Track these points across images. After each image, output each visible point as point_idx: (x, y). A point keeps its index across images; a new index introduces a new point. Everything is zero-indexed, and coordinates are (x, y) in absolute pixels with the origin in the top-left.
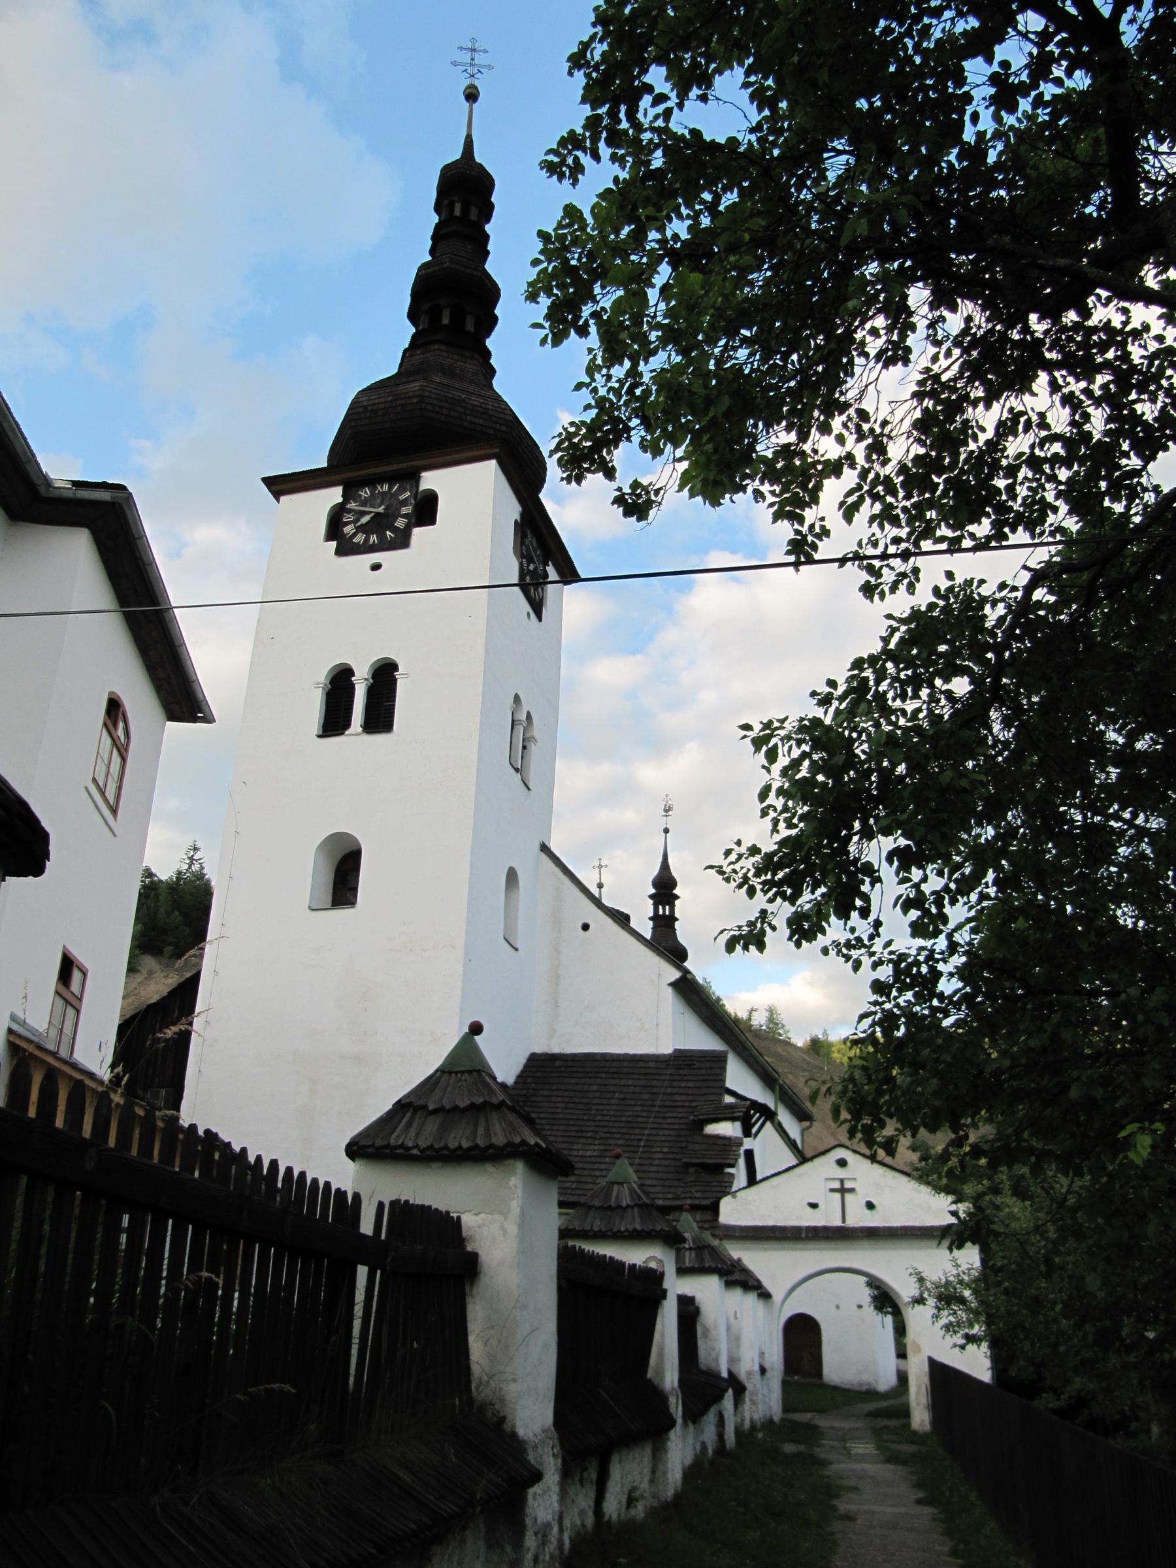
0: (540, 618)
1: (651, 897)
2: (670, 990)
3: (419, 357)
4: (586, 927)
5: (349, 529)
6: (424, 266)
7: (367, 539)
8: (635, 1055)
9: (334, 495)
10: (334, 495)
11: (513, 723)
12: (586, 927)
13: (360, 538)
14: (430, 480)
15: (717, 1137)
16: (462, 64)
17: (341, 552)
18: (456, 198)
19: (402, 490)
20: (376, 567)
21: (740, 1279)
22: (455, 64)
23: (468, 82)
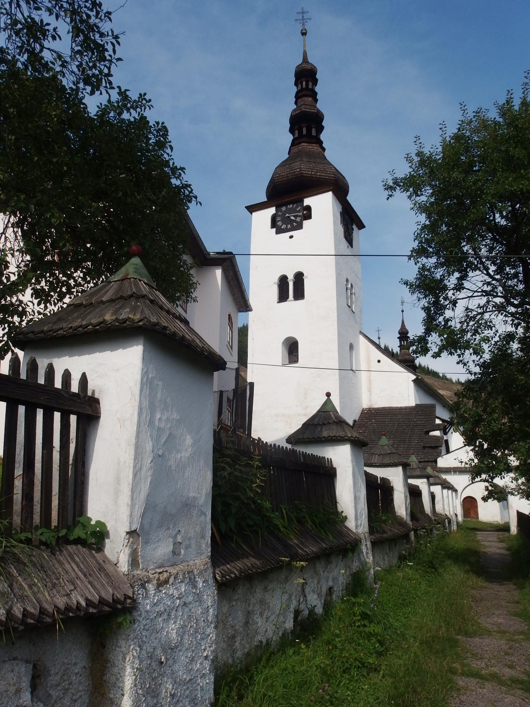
0: (352, 247)
1: (398, 338)
2: (412, 382)
3: (295, 149)
4: (379, 361)
5: (279, 223)
6: (294, 110)
7: (287, 226)
8: (401, 407)
9: (272, 210)
10: (272, 210)
11: (347, 289)
12: (379, 361)
13: (284, 227)
14: (307, 202)
15: (434, 436)
16: (299, 20)
17: (277, 233)
18: (303, 80)
19: (297, 207)
20: (291, 237)
21: (447, 486)
22: (296, 20)
23: (302, 28)
